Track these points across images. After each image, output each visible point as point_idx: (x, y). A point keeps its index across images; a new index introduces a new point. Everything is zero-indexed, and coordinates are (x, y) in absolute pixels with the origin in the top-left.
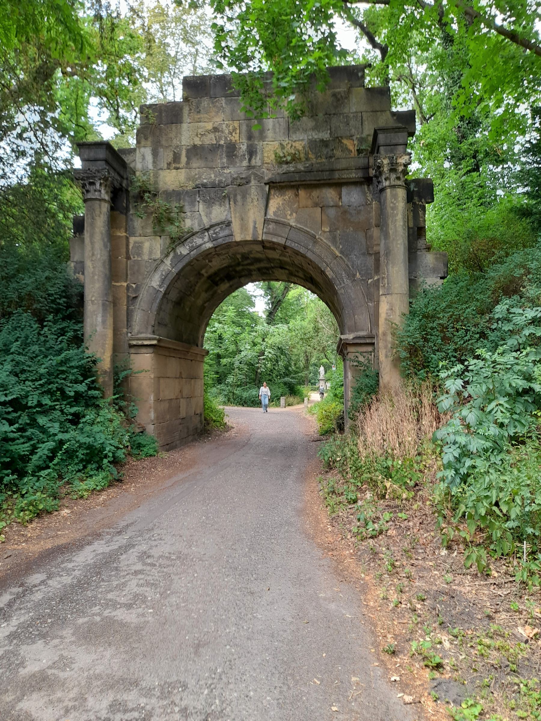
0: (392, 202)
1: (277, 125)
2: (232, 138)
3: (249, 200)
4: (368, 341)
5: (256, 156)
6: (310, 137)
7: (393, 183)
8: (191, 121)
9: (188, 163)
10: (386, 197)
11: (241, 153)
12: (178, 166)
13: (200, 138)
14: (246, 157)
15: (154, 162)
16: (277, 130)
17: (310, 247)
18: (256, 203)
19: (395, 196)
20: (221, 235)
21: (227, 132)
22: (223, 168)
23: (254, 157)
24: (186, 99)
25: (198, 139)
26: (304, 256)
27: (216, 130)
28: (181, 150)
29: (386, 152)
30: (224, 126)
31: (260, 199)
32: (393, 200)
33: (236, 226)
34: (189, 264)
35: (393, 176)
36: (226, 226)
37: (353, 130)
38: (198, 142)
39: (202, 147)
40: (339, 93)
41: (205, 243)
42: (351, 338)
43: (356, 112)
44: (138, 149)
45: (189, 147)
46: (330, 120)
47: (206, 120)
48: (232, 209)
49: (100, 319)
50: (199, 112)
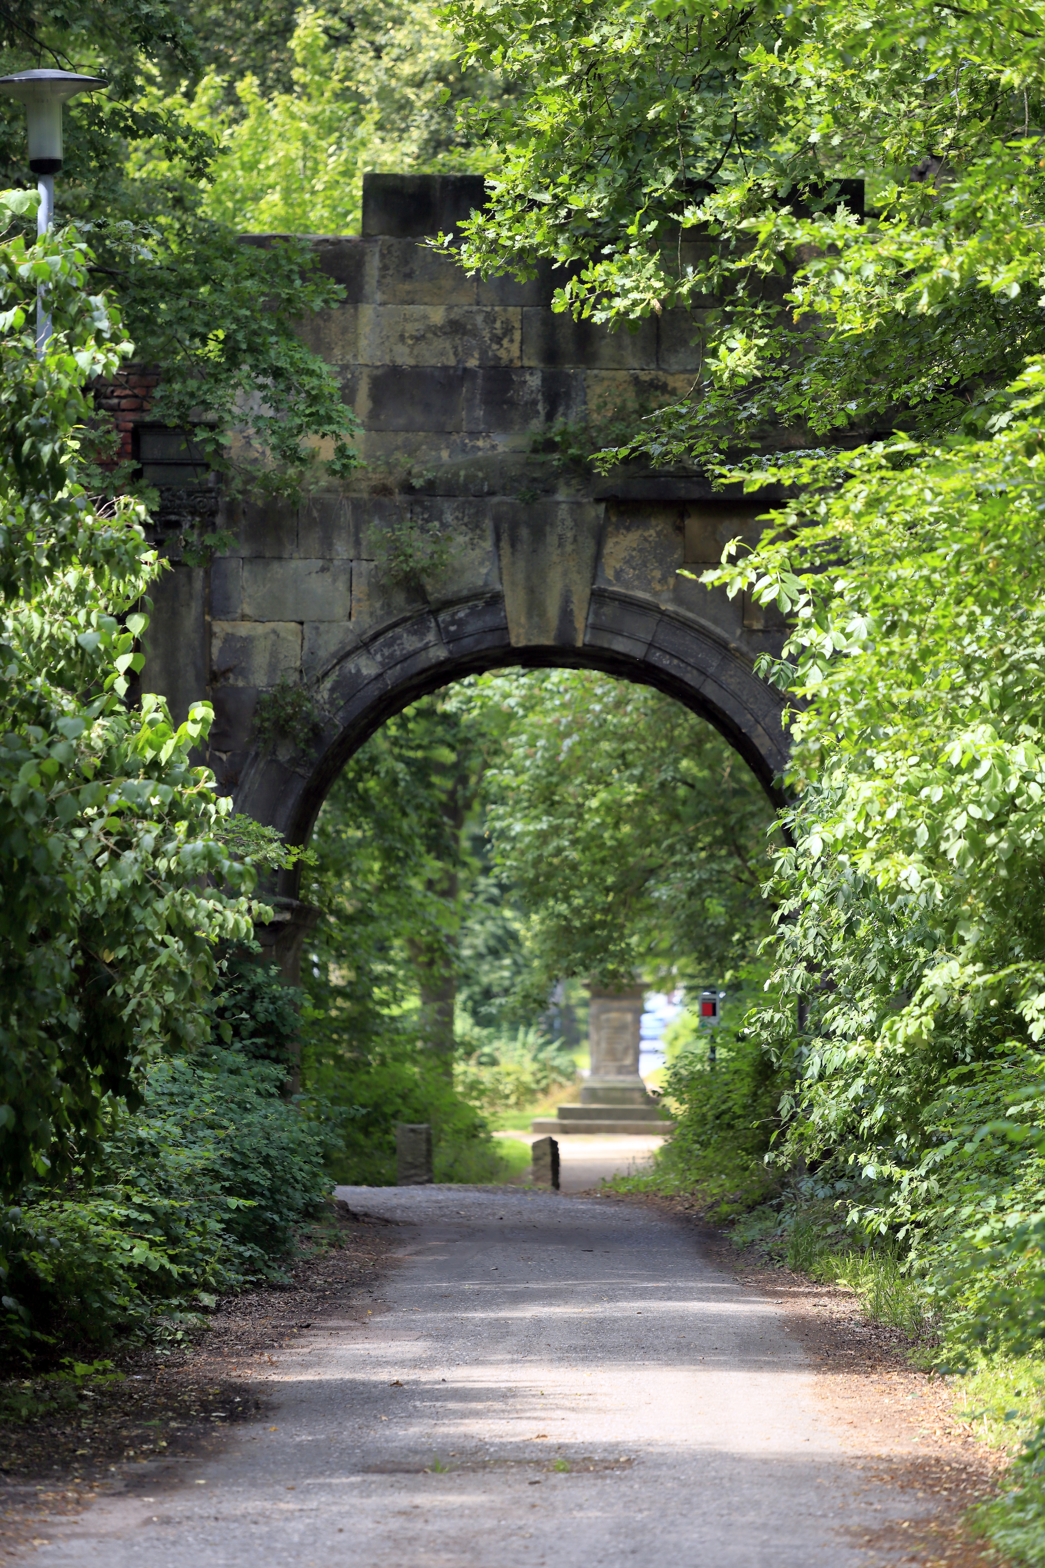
2: (502, 353)
5: (568, 407)
8: (385, 297)
9: (373, 415)
11: (527, 397)
13: (412, 347)
14: (540, 407)
17: (711, 670)
18: (569, 548)
20: (470, 628)
21: (486, 334)
22: (474, 434)
23: (561, 409)
24: (366, 235)
25: (407, 350)
30: (479, 319)
31: (580, 539)
38: (404, 358)
39: (418, 374)
41: (426, 648)
45: (379, 372)
47: (426, 300)
48: (505, 561)
50: (409, 276)
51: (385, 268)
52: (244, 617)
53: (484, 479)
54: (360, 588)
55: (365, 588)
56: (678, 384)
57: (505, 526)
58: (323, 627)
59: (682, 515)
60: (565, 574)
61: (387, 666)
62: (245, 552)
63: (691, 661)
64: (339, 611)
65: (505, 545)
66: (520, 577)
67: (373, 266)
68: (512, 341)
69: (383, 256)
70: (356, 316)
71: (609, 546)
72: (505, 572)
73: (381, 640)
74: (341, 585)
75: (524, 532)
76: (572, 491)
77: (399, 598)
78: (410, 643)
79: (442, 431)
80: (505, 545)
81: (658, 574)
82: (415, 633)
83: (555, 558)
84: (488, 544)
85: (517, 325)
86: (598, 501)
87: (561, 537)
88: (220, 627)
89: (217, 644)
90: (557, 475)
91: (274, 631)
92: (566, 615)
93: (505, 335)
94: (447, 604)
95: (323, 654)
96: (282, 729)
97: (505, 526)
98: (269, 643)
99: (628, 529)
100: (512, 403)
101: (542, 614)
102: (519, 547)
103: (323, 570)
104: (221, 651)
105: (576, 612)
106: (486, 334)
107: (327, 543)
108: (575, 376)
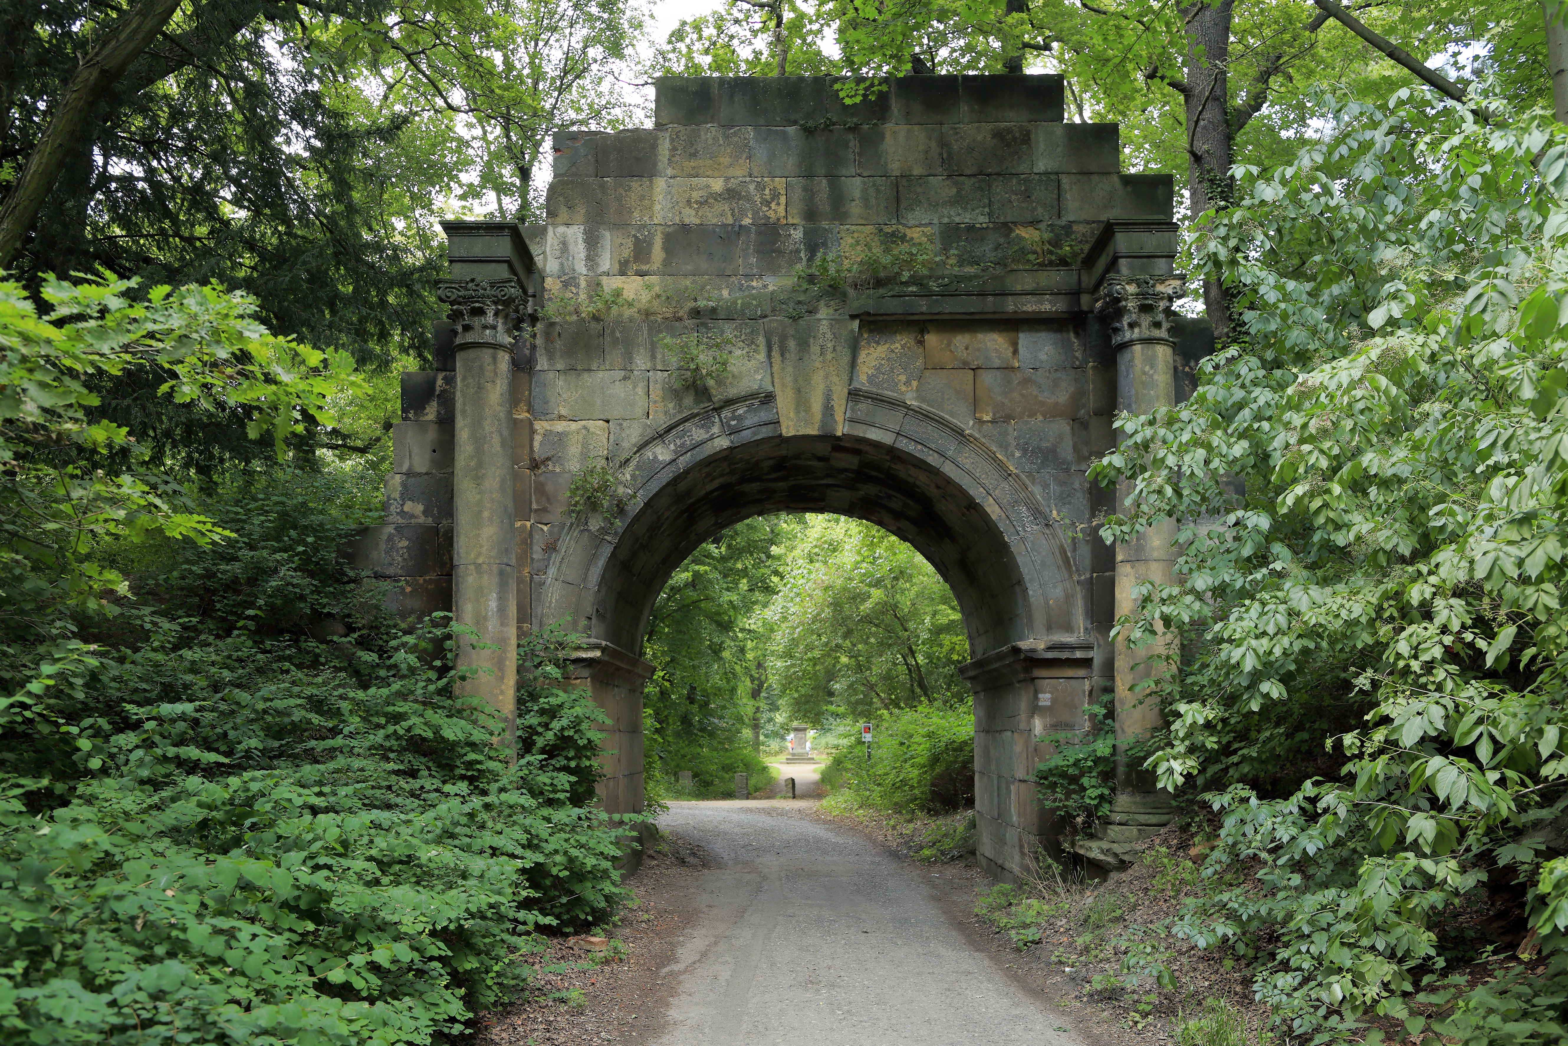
0: (1144, 373)
1: (872, 191)
2: (771, 214)
3: (815, 349)
4: (1079, 655)
6: (946, 220)
7: (1146, 334)
9: (666, 263)
10: (1132, 360)
11: (791, 247)
12: (645, 268)
14: (802, 255)
15: (589, 258)
16: (873, 201)
17: (950, 453)
18: (829, 356)
19: (1151, 361)
20: (748, 423)
21: (757, 199)
22: (749, 276)
26: (934, 472)
27: (731, 194)
28: (651, 236)
29: (1131, 268)
30: (752, 187)
31: (838, 348)
32: (1147, 368)
33: (784, 403)
34: (674, 482)
35: (1146, 320)
36: (762, 403)
37: (1040, 210)
38: (691, 217)
39: (702, 230)
40: (1009, 131)
41: (711, 439)
42: (1042, 646)
43: (1046, 173)
44: (550, 229)
45: (671, 230)
46: (990, 186)
47: (709, 173)
48: (776, 368)
49: (493, 605)
50: (694, 155)
51: (674, 149)
52: (560, 418)
53: (757, 306)
54: (656, 392)
55: (659, 392)
56: (915, 235)
57: (775, 339)
58: (625, 424)
59: (922, 332)
60: (826, 377)
61: (679, 454)
62: (560, 366)
63: (933, 446)
64: (639, 411)
65: (776, 354)
66: (789, 380)
67: (664, 147)
68: (778, 204)
69: (672, 140)
70: (651, 187)
71: (862, 356)
72: (776, 376)
73: (674, 432)
74: (640, 390)
75: (792, 344)
76: (831, 311)
77: (688, 400)
78: (698, 434)
79: (723, 275)
80: (776, 354)
81: (903, 378)
82: (702, 427)
83: (818, 364)
84: (762, 356)
85: (783, 192)
86: (853, 317)
87: (822, 347)
88: (539, 426)
89: (538, 439)
90: (819, 298)
91: (585, 427)
92: (828, 410)
93: (773, 199)
94: (730, 402)
95: (625, 444)
96: (592, 504)
97: (775, 339)
98: (581, 437)
99: (878, 343)
100: (780, 252)
101: (808, 410)
102: (787, 356)
103: (625, 378)
104: (541, 443)
105: (836, 407)
106: (757, 199)
107: (629, 357)
108: (830, 231)
